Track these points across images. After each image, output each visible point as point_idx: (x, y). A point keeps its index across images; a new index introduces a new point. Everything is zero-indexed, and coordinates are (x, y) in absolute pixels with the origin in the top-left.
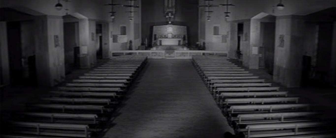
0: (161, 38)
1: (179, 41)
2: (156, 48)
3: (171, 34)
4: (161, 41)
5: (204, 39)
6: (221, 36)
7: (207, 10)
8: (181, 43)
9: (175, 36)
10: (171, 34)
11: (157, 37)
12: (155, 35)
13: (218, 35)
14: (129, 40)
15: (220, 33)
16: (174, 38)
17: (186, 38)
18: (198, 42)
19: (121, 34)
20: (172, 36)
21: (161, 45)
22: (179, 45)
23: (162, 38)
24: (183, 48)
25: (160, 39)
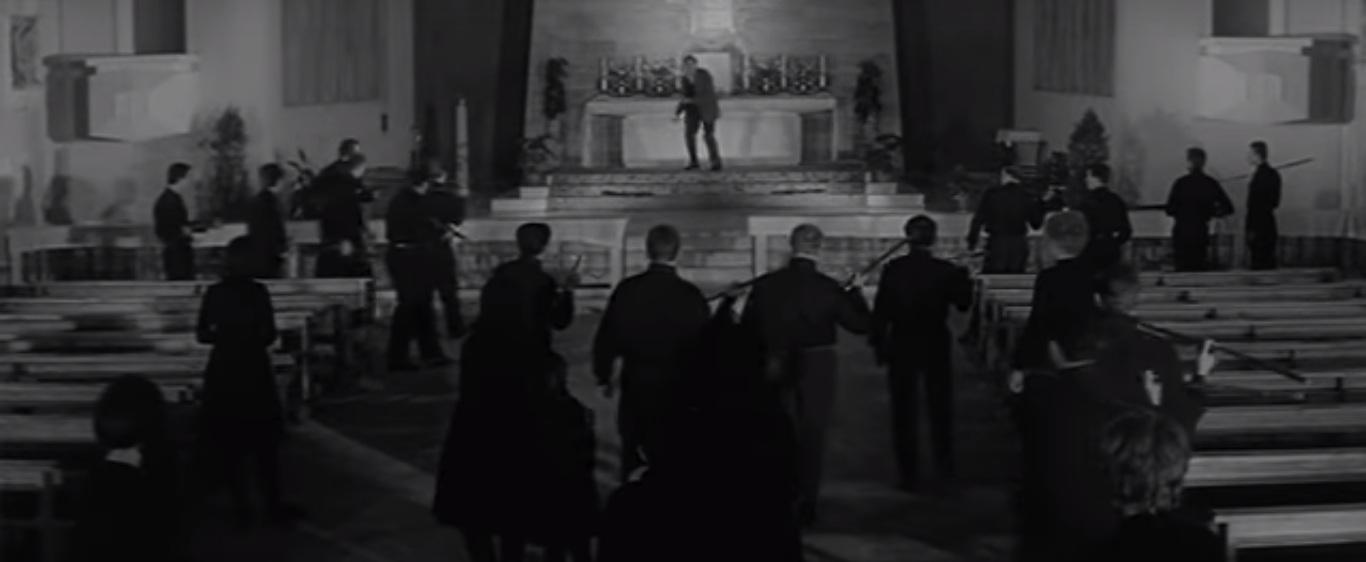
0: (613, 92)
1: (812, 125)
2: (1128, 275)
3: (729, 49)
4: (612, 128)
5: (1099, 75)
6: (1295, 46)
7: (630, 247)
8: (838, 141)
9: (770, 73)
10: (729, 49)
11: (571, 85)
12: (555, 70)
13: (1260, 31)
14: (219, 107)
15: (1276, 25)
16: (757, 90)
17: (891, 96)
18: (1009, 124)
19: (143, 49)
20: (738, 80)
21: (613, 162)
22: (811, 159)
23: (631, 92)
24: (857, 185)
25: (599, 107)
